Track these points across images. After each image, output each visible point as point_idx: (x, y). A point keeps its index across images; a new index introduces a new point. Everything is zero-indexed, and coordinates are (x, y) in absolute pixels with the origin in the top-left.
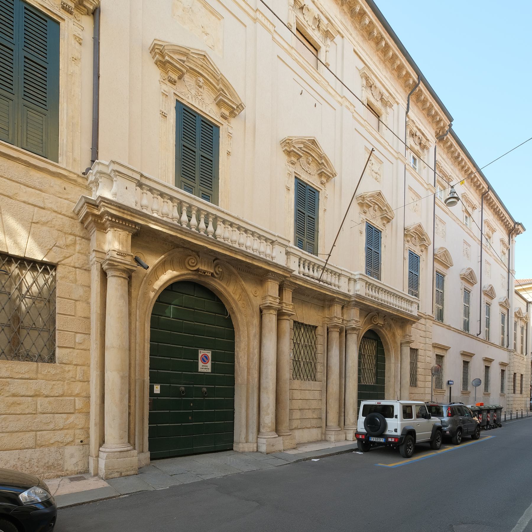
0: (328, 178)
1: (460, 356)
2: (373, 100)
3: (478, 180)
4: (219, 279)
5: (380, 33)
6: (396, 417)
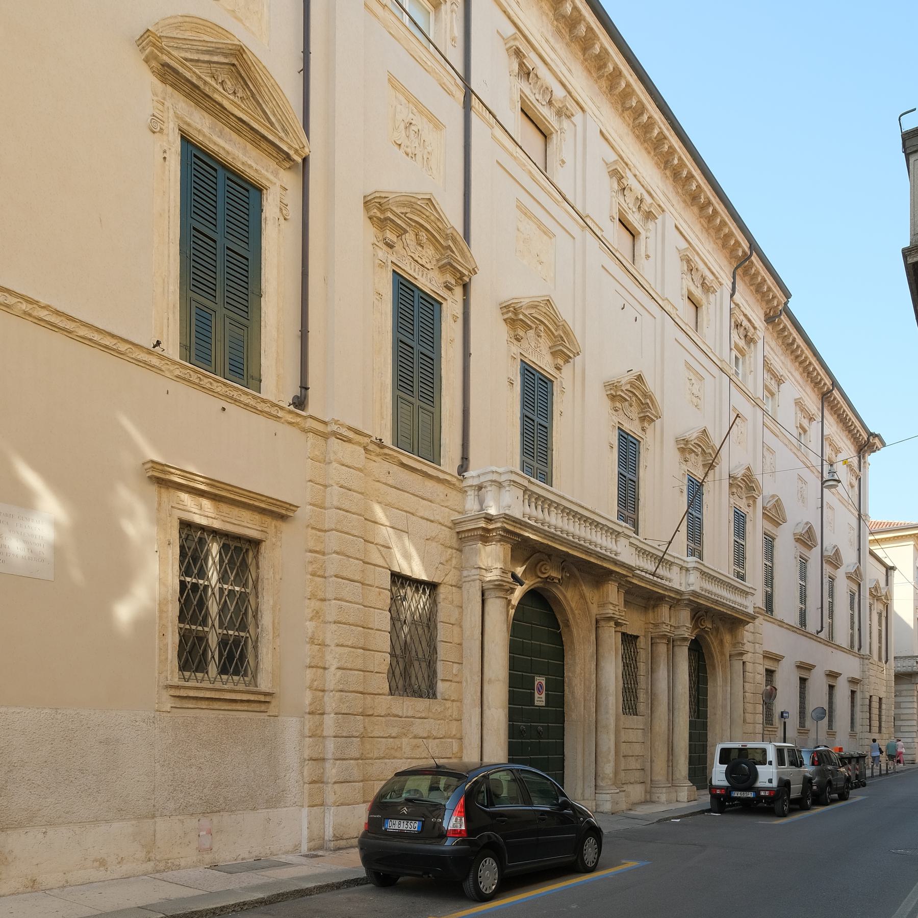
0: (567, 359)
1: (795, 670)
2: (693, 289)
3: (818, 374)
5: (708, 198)
6: (770, 763)
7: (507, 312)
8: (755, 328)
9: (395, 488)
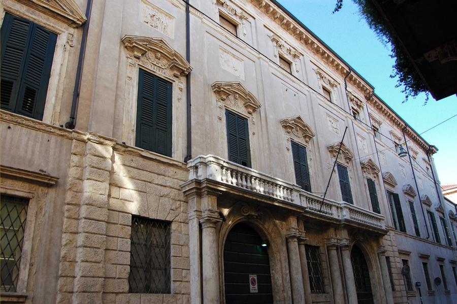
0: (310, 138)
4: (260, 219)
7: (215, 88)
8: (361, 102)
9: (137, 168)
